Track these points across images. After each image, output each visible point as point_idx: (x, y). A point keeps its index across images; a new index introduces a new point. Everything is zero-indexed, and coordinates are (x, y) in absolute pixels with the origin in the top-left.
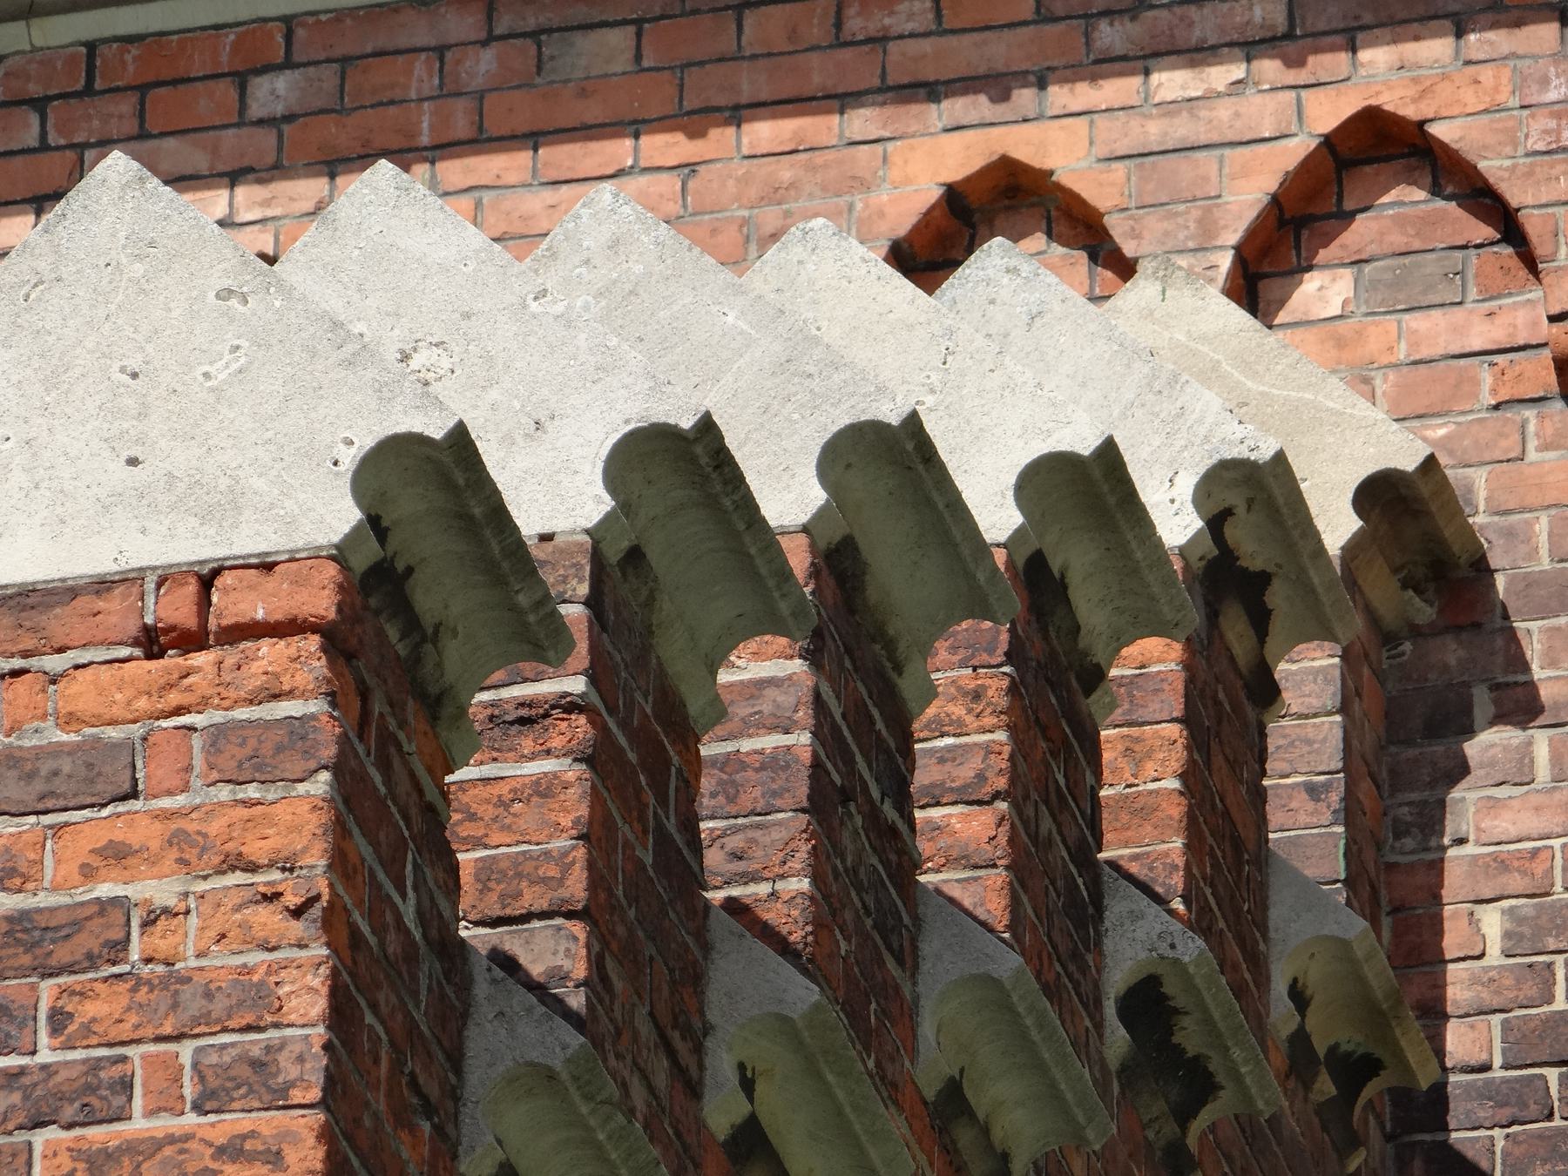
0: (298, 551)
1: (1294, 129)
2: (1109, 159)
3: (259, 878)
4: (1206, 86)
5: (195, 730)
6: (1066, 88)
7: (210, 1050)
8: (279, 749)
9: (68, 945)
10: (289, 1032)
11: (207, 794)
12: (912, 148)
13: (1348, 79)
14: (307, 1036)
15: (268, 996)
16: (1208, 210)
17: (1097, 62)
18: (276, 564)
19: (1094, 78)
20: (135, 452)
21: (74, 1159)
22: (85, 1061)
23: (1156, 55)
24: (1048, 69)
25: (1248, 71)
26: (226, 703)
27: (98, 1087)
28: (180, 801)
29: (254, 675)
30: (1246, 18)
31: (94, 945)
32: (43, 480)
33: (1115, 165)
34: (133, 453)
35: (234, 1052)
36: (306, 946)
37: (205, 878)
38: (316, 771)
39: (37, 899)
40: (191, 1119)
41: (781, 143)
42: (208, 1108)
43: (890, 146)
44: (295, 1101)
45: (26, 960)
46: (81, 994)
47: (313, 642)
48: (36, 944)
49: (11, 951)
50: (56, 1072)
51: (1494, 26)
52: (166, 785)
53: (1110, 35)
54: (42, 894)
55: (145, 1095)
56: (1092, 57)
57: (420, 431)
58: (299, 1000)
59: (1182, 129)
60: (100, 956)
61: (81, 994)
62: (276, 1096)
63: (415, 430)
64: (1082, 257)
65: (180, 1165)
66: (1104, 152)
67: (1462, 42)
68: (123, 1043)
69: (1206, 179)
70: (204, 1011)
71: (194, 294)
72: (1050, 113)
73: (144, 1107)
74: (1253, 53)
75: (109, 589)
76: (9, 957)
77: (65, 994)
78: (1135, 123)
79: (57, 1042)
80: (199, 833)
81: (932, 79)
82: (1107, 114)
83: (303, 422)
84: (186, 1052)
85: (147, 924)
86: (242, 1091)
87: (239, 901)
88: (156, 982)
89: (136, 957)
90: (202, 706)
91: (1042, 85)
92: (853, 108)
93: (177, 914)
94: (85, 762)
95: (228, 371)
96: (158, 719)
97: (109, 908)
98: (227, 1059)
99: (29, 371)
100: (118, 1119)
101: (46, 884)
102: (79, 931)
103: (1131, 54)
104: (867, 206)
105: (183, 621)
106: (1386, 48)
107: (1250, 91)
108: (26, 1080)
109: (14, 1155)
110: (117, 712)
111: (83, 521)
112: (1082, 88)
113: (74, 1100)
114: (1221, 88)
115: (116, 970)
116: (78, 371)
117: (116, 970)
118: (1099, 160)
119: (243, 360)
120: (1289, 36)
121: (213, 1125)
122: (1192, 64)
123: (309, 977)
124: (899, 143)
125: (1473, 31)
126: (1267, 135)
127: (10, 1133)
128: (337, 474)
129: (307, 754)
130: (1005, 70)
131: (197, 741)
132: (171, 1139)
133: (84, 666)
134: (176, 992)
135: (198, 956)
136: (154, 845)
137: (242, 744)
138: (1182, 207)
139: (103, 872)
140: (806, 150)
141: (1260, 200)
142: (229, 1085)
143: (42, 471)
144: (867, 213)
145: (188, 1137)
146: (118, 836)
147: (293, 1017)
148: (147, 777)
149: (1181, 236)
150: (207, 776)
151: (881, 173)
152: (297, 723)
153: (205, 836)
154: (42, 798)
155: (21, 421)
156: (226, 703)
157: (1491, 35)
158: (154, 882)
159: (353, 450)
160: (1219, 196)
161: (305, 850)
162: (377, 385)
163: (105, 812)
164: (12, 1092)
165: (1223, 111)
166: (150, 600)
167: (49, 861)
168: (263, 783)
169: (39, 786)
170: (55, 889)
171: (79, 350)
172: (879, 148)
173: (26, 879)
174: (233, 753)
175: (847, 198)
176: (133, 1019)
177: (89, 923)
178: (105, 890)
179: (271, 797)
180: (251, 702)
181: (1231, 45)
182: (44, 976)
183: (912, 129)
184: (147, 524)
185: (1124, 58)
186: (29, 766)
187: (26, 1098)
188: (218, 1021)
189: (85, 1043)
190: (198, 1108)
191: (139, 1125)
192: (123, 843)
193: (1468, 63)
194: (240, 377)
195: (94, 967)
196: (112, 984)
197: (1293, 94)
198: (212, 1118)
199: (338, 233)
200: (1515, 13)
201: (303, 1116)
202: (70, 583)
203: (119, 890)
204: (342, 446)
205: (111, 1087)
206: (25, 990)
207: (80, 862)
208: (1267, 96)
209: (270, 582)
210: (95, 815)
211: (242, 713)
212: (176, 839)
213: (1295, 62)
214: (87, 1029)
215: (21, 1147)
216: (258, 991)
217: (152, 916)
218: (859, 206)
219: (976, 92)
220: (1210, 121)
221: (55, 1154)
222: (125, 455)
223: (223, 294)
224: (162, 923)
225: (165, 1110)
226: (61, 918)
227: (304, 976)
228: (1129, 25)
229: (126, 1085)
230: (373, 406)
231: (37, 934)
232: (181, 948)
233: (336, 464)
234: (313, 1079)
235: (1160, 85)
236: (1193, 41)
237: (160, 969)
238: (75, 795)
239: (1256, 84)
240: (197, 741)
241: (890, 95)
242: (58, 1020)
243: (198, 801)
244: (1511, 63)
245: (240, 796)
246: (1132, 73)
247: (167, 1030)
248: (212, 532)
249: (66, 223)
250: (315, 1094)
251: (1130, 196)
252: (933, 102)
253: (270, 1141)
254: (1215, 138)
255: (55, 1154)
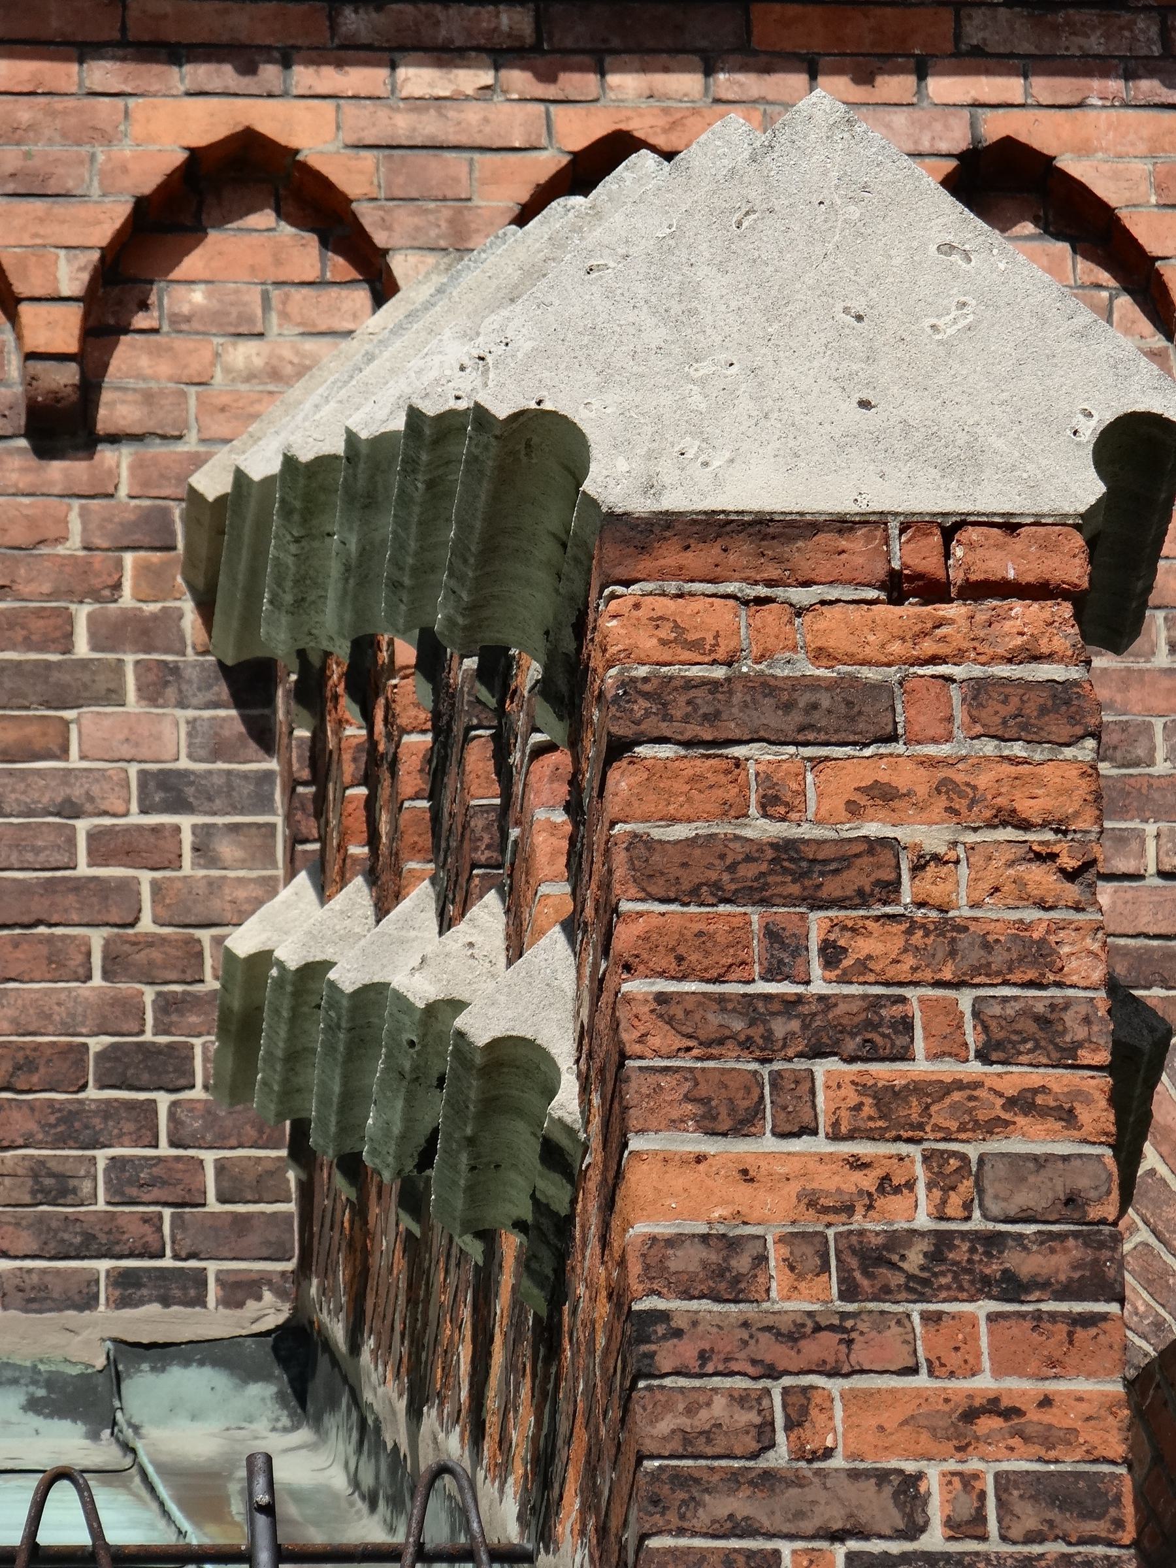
0: (1043, 516)
1: (544, 142)
2: (357, 147)
3: (1030, 837)
4: (454, 87)
5: (954, 681)
6: (311, 70)
7: (992, 1001)
8: (1043, 711)
9: (838, 880)
10: (1070, 992)
11: (971, 746)
12: (155, 107)
13: (596, 100)
14: (1092, 999)
15: (1051, 955)
16: (459, 212)
17: (343, 47)
18: (1020, 525)
19: (340, 64)
20: (866, 395)
21: (860, 1094)
22: (864, 997)
23: (403, 49)
24: (293, 47)
25: (496, 78)
26: (983, 659)
27: (880, 1025)
28: (944, 750)
29: (1008, 634)
30: (493, 25)
31: (866, 884)
32: (772, 410)
33: (364, 153)
34: (865, 396)
35: (1017, 1006)
36: (1083, 910)
37: (975, 830)
38: (1083, 737)
39: (800, 830)
40: (975, 1068)
41: (19, 83)
42: (994, 1057)
43: (132, 102)
44: (1085, 1062)
45: (795, 889)
46: (853, 930)
47: (1066, 609)
48: (805, 874)
49: (779, 879)
50: (836, 1005)
51: (744, 68)
52: (931, 733)
53: (354, 21)
54: (806, 826)
55: (926, 1038)
56: (336, 41)
57: (1160, 412)
58: (1079, 962)
59: (429, 127)
60: (872, 895)
61: (853, 930)
62: (1065, 1054)
63: (1154, 411)
64: (312, 239)
65: (970, 1111)
66: (352, 139)
67: (711, 80)
68: (901, 984)
69: (456, 180)
70: (983, 961)
71: (915, 244)
72: (295, 92)
73: (927, 1050)
74: (500, 61)
75: (851, 529)
76: (777, 884)
77: (837, 929)
78: (382, 114)
79: (832, 975)
80: (968, 784)
81: (173, 40)
82: (353, 101)
83: (1038, 388)
84: (965, 999)
85: (917, 868)
86: (1029, 1045)
87: (1012, 857)
88: (932, 927)
89: (908, 900)
90: (958, 658)
91: (287, 64)
92: (93, 59)
93: (947, 862)
94: (844, 699)
95: (956, 327)
96: (912, 665)
97: (878, 849)
98: (1010, 1012)
99: (748, 299)
100: (903, 1059)
101: (810, 816)
102: (848, 867)
103: (376, 44)
104: (109, 159)
105: (932, 571)
106: (635, 76)
107: (499, 98)
108: (804, 1009)
109: (797, 1082)
110: (869, 652)
111: (815, 458)
112: (328, 71)
113: (856, 1034)
114: (470, 92)
115: (888, 910)
116: (799, 306)
117: (888, 910)
118: (347, 146)
119: (971, 318)
120: (536, 48)
121: (999, 1075)
122: (440, 64)
123: (1089, 941)
124: (141, 100)
125: (722, 70)
126: (517, 145)
127: (790, 1060)
128: (1078, 444)
129: (1073, 720)
130: (248, 42)
131: (955, 691)
132: (959, 1085)
133: (831, 603)
134: (953, 939)
135: (972, 907)
136: (922, 791)
137: (1005, 702)
138: (432, 205)
139: (870, 811)
140: (44, 94)
141: (511, 209)
142: (1015, 1038)
143: (770, 402)
144: (109, 166)
145: (977, 1085)
146: (884, 777)
147: (1075, 979)
148: (907, 721)
149: (433, 233)
150: (969, 729)
151: (122, 128)
152: (1060, 687)
153: (974, 788)
154: (802, 729)
155: (744, 348)
156: (983, 659)
157: (741, 77)
158: (924, 828)
159: (1093, 423)
160: (469, 199)
161: (1077, 814)
162: (1112, 361)
163: (868, 752)
164: (789, 1019)
165: (473, 114)
166: (895, 546)
167: (811, 793)
168: (1029, 742)
169: (797, 718)
170: (818, 822)
171: (798, 286)
172: (119, 102)
173: (790, 808)
174: (994, 713)
175: (88, 148)
176: (910, 961)
177: (858, 861)
178: (873, 829)
179: (1038, 757)
180: (1010, 661)
181: (479, 49)
182: (812, 908)
183: (154, 88)
184: (884, 468)
185: (369, 47)
186: (785, 697)
187: (805, 1027)
188: (998, 973)
189: (861, 979)
190: (983, 1056)
191: (921, 1067)
192: (889, 785)
193: (717, 101)
194: (970, 334)
195: (865, 904)
196: (883, 925)
197: (541, 107)
198: (998, 1068)
199: (692, 182)
200: (763, 59)
201: (1092, 1077)
202: (809, 517)
203: (889, 832)
204: (1081, 417)
205: (893, 1026)
206: (795, 918)
207: (846, 797)
208: (517, 107)
209: (1018, 544)
210: (857, 754)
211: (1003, 671)
212: (944, 787)
213: (547, 76)
214: (863, 965)
215: (804, 1074)
216: (1039, 949)
217: (922, 861)
218: (101, 158)
219: (220, 60)
220: (459, 123)
221: (839, 1086)
222: (856, 397)
223: (944, 248)
224: (931, 869)
225: (950, 1055)
226: (825, 853)
227: (1083, 939)
228: (374, 15)
229: (906, 1025)
230: (1110, 381)
231: (804, 864)
232: (954, 896)
233: (1075, 433)
234: (1102, 1042)
235: (407, 79)
236: (440, 41)
237: (934, 914)
238: (836, 731)
239: (504, 92)
240: (955, 691)
241: (130, 50)
242: (831, 954)
243: (964, 752)
244: (762, 108)
245: (1006, 753)
246: (378, 64)
247: (947, 975)
248: (953, 485)
249: (775, 155)
250: (1103, 1057)
251: (379, 186)
252: (174, 64)
253: (1061, 1097)
254: (464, 140)
255: (839, 1086)
